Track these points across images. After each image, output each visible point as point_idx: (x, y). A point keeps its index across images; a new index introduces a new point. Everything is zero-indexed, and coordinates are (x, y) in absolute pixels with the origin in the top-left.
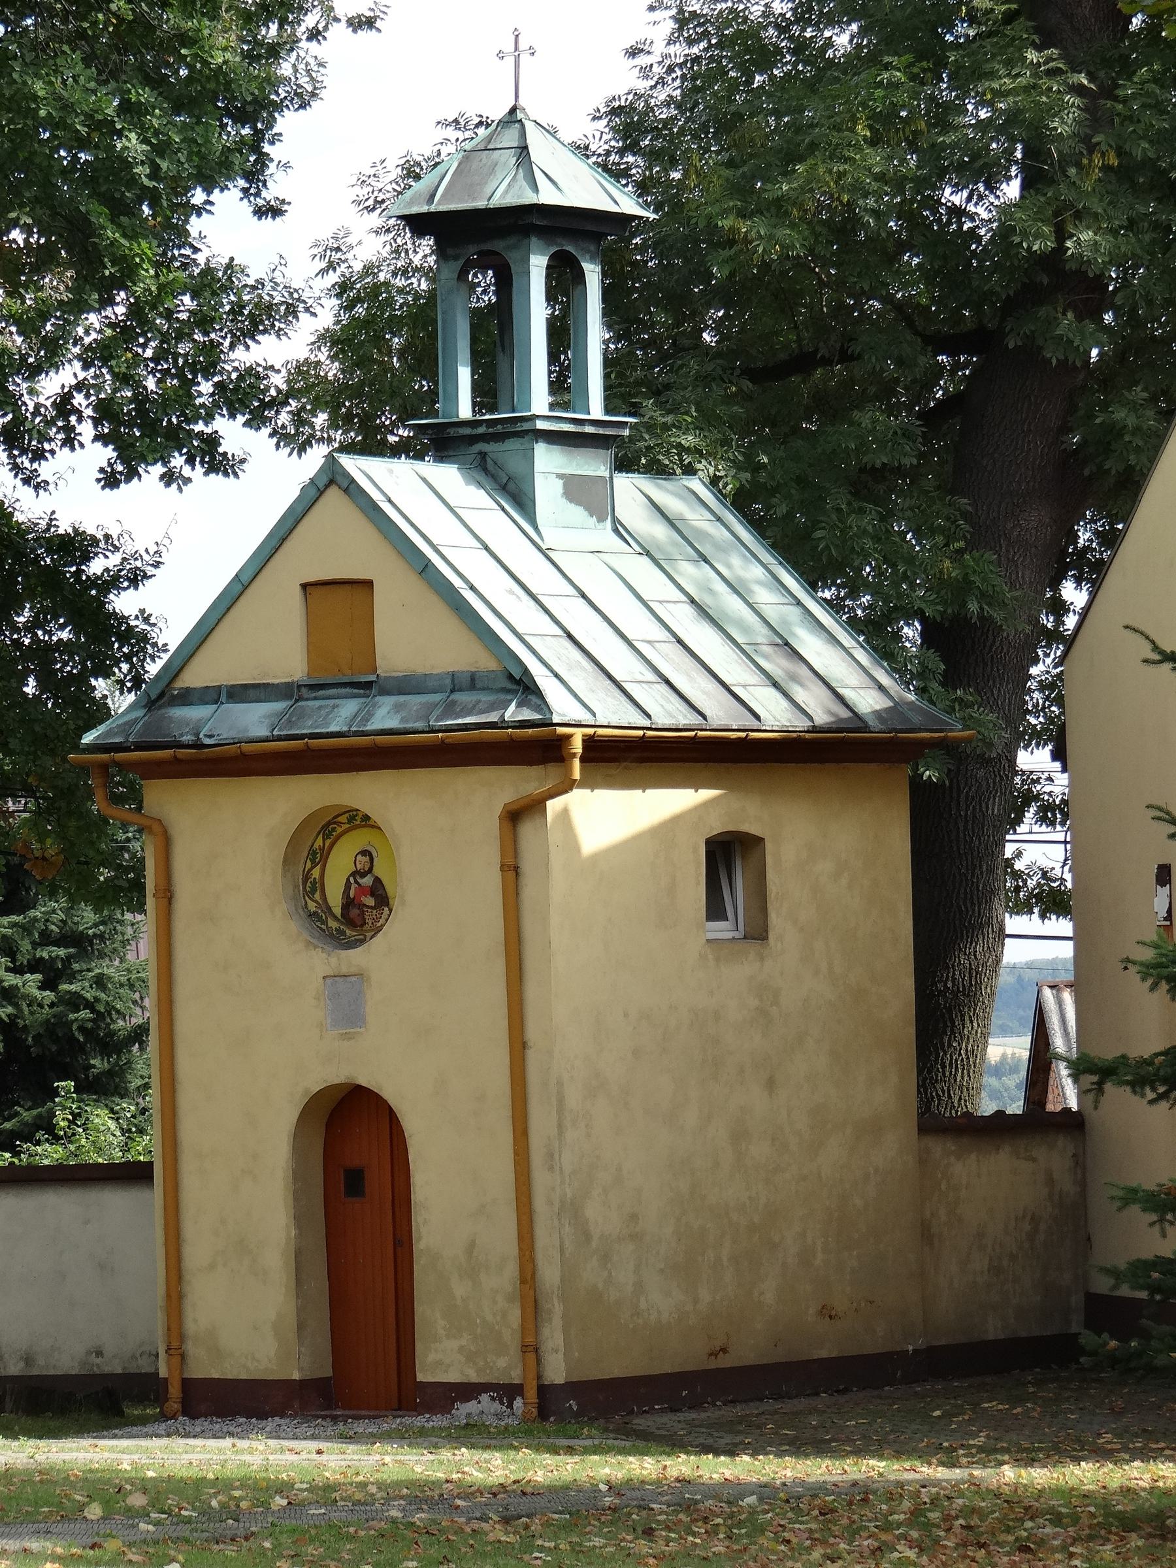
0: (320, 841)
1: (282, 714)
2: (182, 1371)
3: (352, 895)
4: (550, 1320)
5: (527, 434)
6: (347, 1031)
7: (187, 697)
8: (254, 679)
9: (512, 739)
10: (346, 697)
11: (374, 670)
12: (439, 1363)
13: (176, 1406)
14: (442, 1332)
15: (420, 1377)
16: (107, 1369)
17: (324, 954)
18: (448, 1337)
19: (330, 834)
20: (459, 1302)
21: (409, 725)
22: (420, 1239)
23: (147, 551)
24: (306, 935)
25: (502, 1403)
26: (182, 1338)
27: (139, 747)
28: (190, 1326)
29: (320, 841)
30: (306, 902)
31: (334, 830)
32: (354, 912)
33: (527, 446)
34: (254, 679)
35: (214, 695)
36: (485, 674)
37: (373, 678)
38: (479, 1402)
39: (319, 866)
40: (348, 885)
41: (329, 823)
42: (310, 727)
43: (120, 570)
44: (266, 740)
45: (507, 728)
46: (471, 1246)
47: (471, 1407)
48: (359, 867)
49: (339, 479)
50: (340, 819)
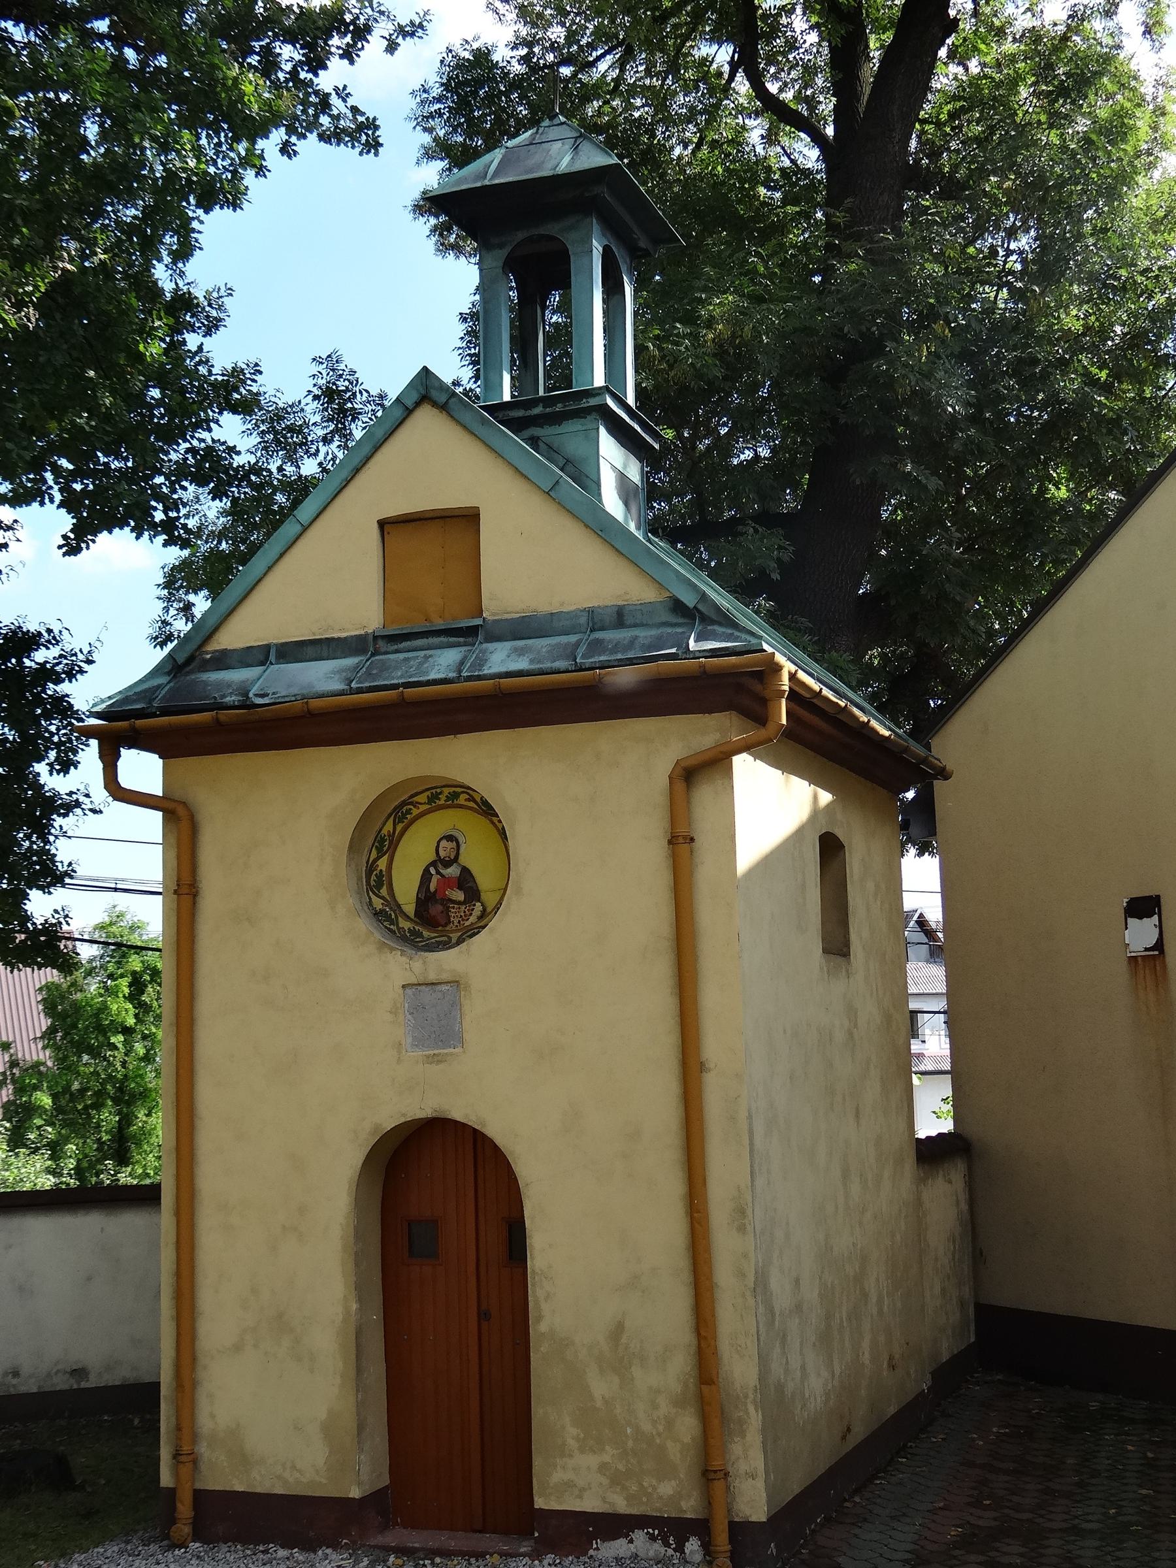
0: (389, 826)
1: (356, 668)
2: (193, 1483)
3: (432, 889)
4: (743, 1434)
5: (589, 414)
6: (436, 1052)
7: (223, 660)
8: (303, 636)
9: (705, 672)
10: (440, 648)
11: (480, 613)
12: (569, 1485)
13: (187, 1530)
14: (572, 1443)
15: (540, 1503)
16: (23, 1389)
17: (404, 959)
18: (582, 1450)
19: (404, 816)
20: (599, 1404)
21: (547, 665)
22: (539, 1318)
23: (81, 651)
24: (377, 936)
25: (668, 1545)
26: (195, 1437)
27: (165, 712)
28: (205, 1423)
29: (389, 826)
30: (370, 898)
31: (409, 812)
32: (435, 910)
33: (590, 426)
34: (314, 634)
35: (261, 655)
36: (639, 607)
37: (478, 622)
38: (631, 1541)
39: (386, 857)
40: (426, 877)
41: (404, 803)
42: (401, 677)
43: (58, 664)
44: (341, 693)
45: (699, 658)
46: (618, 1331)
47: (619, 1547)
48: (442, 854)
49: (434, 394)
50: (416, 799)
